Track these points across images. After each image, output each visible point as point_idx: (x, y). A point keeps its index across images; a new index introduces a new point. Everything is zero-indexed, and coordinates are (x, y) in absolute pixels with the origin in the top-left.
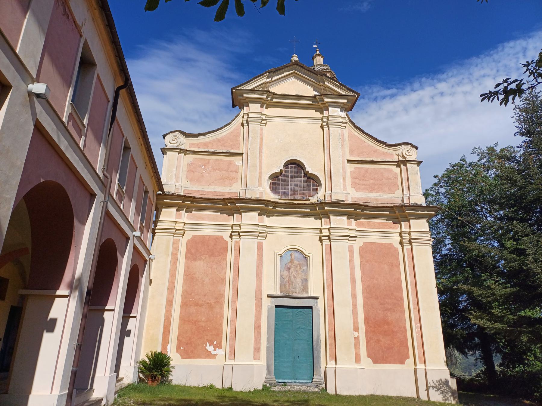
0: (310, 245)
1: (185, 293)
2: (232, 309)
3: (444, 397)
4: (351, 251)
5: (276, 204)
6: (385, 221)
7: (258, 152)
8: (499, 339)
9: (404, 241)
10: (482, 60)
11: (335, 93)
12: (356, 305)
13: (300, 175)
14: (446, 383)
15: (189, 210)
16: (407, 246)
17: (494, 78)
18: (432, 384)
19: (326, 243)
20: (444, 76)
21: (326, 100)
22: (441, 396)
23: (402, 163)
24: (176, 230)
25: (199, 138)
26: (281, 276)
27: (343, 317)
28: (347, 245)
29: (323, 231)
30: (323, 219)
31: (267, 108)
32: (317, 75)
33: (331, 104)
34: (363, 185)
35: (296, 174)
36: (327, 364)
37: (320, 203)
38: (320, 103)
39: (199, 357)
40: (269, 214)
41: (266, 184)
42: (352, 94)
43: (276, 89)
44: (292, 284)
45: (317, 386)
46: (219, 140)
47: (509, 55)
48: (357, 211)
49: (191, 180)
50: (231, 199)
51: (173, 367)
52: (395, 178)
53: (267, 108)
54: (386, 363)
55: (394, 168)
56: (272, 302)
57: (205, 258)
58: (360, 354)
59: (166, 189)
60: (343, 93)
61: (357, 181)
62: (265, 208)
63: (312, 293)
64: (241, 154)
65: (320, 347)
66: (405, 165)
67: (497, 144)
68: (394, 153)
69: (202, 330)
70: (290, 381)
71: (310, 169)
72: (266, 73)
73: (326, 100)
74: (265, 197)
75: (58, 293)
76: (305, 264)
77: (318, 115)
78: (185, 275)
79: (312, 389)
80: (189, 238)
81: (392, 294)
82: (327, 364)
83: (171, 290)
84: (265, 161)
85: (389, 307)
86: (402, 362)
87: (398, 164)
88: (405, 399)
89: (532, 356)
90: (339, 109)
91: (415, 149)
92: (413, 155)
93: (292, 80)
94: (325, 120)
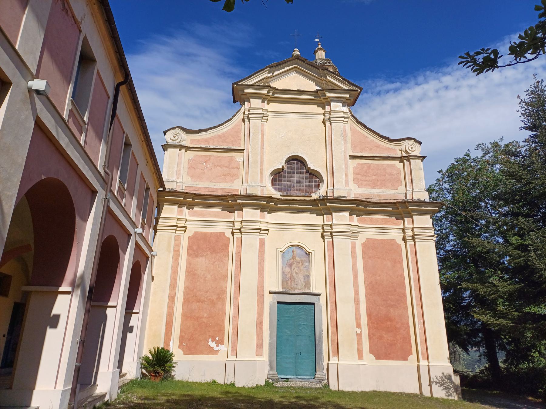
0: (312, 241)
2: (234, 305)
3: (447, 393)
4: (353, 247)
6: (388, 217)
9: (407, 237)
12: (359, 302)
13: (302, 171)
14: (449, 378)
15: (190, 206)
16: (410, 243)
18: (435, 380)
19: (328, 239)
20: (449, 69)
21: (328, 95)
22: (444, 392)
23: (405, 158)
24: (177, 227)
25: (200, 134)
26: (283, 272)
27: (346, 314)
28: (349, 241)
30: (325, 216)
31: (268, 103)
32: (319, 69)
34: (365, 181)
36: (329, 360)
38: (322, 98)
39: (201, 353)
40: (271, 211)
41: (268, 180)
42: (355, 88)
43: (278, 84)
44: (294, 281)
45: (319, 382)
46: (220, 136)
48: (359, 207)
49: (192, 177)
51: (175, 363)
52: (399, 174)
53: (268, 103)
54: (389, 359)
55: (397, 163)
56: (274, 299)
59: (168, 186)
60: (346, 88)
61: (359, 177)
62: (266, 204)
64: (242, 151)
65: (322, 343)
66: (409, 161)
67: (502, 139)
68: (397, 148)
69: (204, 326)
70: (292, 377)
71: (312, 166)
72: (267, 68)
73: (328, 95)
74: (266, 194)
75: (61, 289)
76: (307, 260)
77: (320, 110)
78: (187, 271)
79: (315, 385)
80: (191, 235)
81: (395, 291)
82: (329, 360)
83: (173, 286)
84: (266, 158)
85: (392, 303)
86: (405, 359)
89: (537, 353)
90: (341, 104)
91: (418, 145)
92: (417, 150)
93: (294, 74)
94: (327, 115)
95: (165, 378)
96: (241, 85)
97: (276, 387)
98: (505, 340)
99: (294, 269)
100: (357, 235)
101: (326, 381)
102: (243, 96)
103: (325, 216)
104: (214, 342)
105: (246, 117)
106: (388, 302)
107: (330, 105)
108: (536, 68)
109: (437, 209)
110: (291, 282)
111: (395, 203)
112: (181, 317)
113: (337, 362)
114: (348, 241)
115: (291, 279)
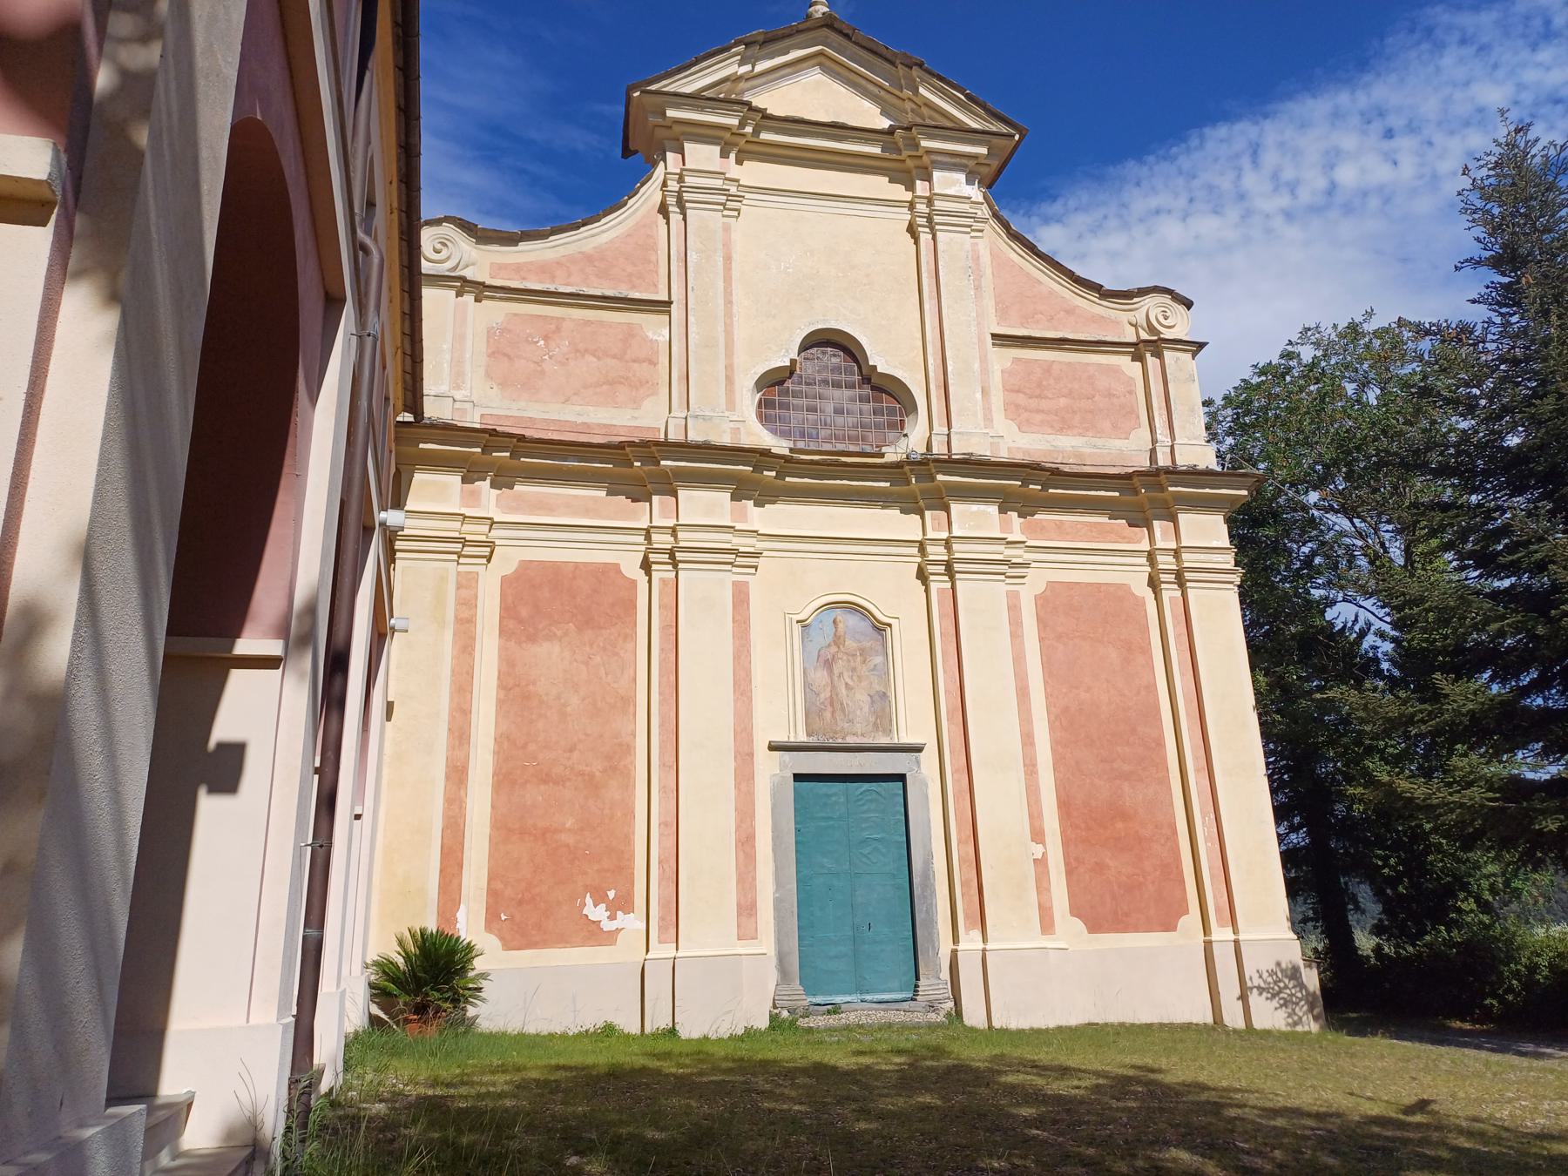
0: (891, 590)
1: (506, 745)
2: (663, 789)
3: (1290, 1016)
4: (1014, 608)
5: (787, 464)
6: (1104, 519)
7: (721, 301)
8: (1378, 857)
9: (1163, 577)
10: (1151, 169)
11: (949, 124)
12: (1034, 765)
13: (850, 378)
14: (1294, 973)
15: (503, 480)
16: (1170, 593)
17: (1184, 219)
18: (1257, 981)
19: (939, 584)
20: (1056, 208)
21: (925, 143)
22: (1282, 1013)
23: (1149, 347)
24: (465, 542)
25: (523, 246)
26: (807, 685)
27: (1000, 803)
28: (1000, 588)
29: (929, 549)
30: (928, 514)
31: (739, 162)
32: (892, 63)
33: (939, 158)
34: (1038, 411)
35: (837, 377)
36: (956, 940)
37: (920, 463)
38: (905, 153)
39: (563, 940)
40: (766, 496)
41: (748, 402)
42: (1004, 129)
43: (777, 99)
44: (843, 710)
45: (932, 1007)
46: (588, 258)
47: (1216, 160)
48: (1029, 486)
49: (504, 384)
50: (645, 444)
51: (484, 976)
52: (1130, 392)
53: (739, 162)
54: (1125, 930)
55: (1124, 362)
56: (783, 766)
57: (566, 634)
58: (1051, 908)
59: (433, 410)
60: (974, 125)
61: (1021, 399)
62: (751, 475)
63: (902, 734)
64: (663, 306)
65: (933, 892)
66: (1158, 355)
67: (1370, 314)
68: (1124, 317)
69: (564, 857)
70: (848, 999)
71: (881, 360)
72: (736, 44)
73: (925, 143)
74: (746, 441)
75: (243, 647)
76: (880, 648)
77: (899, 192)
78: (503, 686)
79: (919, 1018)
80: (510, 569)
81: (1133, 731)
82: (956, 940)
83: (460, 735)
84: (740, 333)
85: (1126, 768)
86: (1169, 927)
87: (1137, 351)
88: (1188, 1027)
89: (1471, 900)
90: (962, 177)
91: (1182, 308)
92: (1179, 325)
93: (815, 77)
94: (922, 207)
95: (454, 1024)
96: (658, 93)
97: (810, 1030)
98: (1386, 870)
99: (841, 674)
100: (1021, 571)
101: (951, 1004)
102: (660, 133)
103: (928, 514)
104: (603, 906)
105: (671, 200)
106: (1115, 765)
107: (929, 179)
108: (1267, 216)
109: (1245, 493)
110: (833, 713)
111: (1128, 476)
112: (487, 830)
113: (981, 946)
114: (997, 590)
115: (832, 704)
